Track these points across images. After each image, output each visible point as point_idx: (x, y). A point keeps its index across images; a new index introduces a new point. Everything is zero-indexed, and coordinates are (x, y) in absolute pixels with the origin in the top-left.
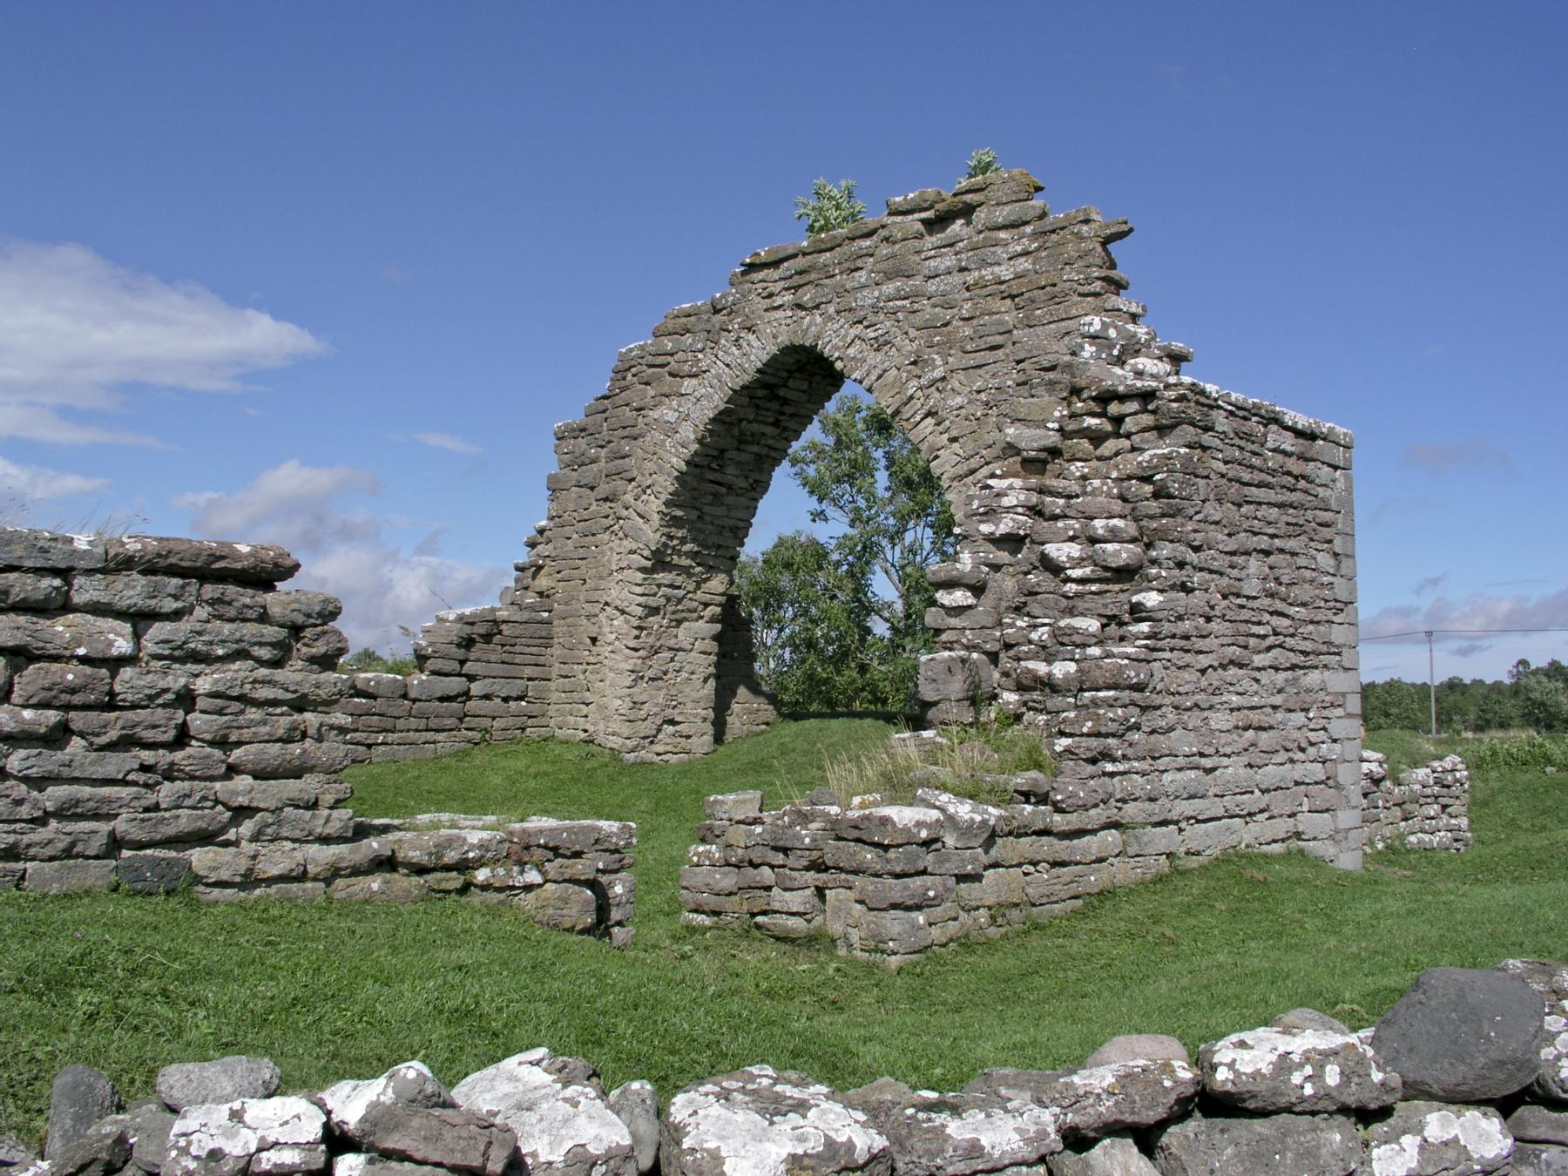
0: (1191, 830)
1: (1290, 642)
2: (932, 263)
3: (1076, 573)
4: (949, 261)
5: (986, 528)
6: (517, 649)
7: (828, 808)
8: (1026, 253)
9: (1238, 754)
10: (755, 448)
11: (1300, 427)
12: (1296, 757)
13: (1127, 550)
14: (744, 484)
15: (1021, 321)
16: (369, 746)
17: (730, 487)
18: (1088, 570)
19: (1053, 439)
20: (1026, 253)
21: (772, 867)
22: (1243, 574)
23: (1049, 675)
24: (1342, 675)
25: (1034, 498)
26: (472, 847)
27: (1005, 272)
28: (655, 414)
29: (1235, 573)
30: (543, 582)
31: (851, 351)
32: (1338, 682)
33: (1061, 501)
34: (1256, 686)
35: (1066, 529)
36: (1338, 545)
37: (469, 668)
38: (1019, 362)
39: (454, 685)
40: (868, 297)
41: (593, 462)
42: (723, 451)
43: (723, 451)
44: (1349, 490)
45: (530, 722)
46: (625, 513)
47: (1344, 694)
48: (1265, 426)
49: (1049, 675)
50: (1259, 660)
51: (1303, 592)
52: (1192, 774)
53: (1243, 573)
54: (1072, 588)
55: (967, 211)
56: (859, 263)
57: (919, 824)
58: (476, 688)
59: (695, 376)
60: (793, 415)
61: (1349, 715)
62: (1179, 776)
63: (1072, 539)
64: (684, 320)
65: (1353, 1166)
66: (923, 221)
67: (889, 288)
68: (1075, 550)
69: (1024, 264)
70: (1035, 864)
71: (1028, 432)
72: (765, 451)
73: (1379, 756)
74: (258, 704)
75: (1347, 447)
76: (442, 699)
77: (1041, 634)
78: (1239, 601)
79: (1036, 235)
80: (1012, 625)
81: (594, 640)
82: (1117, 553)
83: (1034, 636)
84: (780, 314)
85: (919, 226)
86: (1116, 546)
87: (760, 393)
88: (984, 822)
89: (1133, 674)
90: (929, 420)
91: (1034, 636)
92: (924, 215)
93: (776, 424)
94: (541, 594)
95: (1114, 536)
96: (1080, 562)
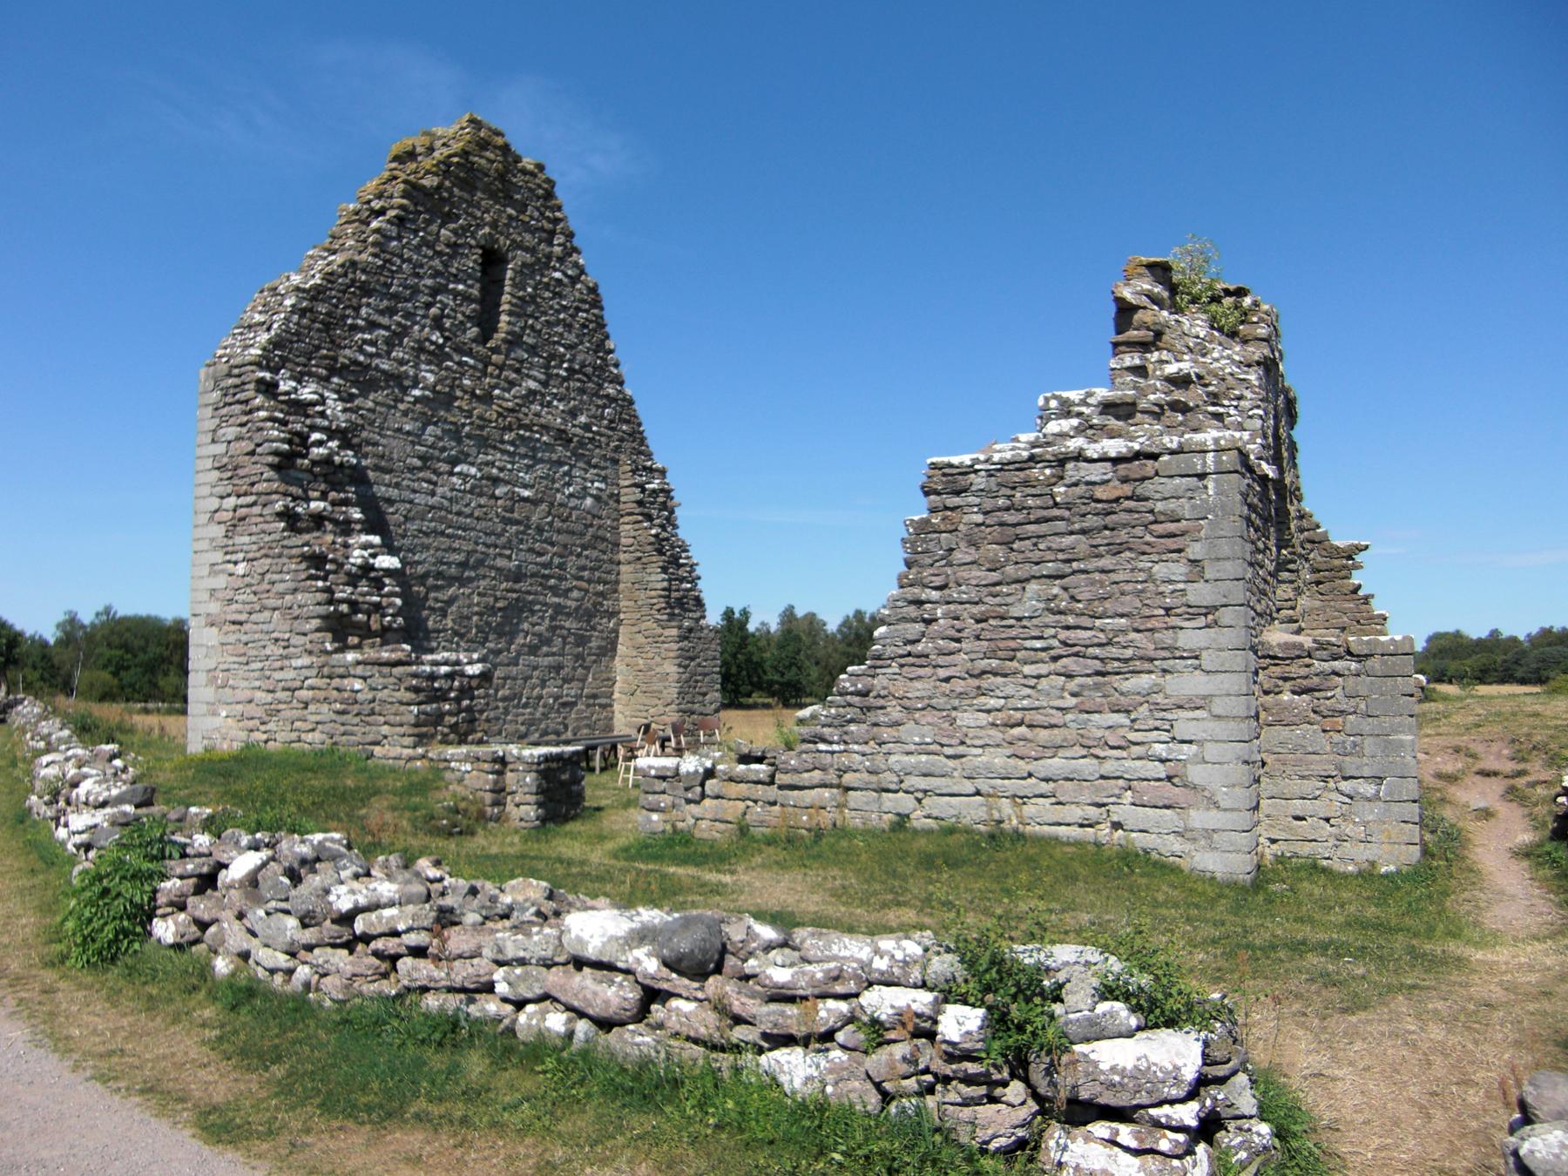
11: (1113, 454)
52: (924, 758)
57: (650, 767)
78: (1005, 623)
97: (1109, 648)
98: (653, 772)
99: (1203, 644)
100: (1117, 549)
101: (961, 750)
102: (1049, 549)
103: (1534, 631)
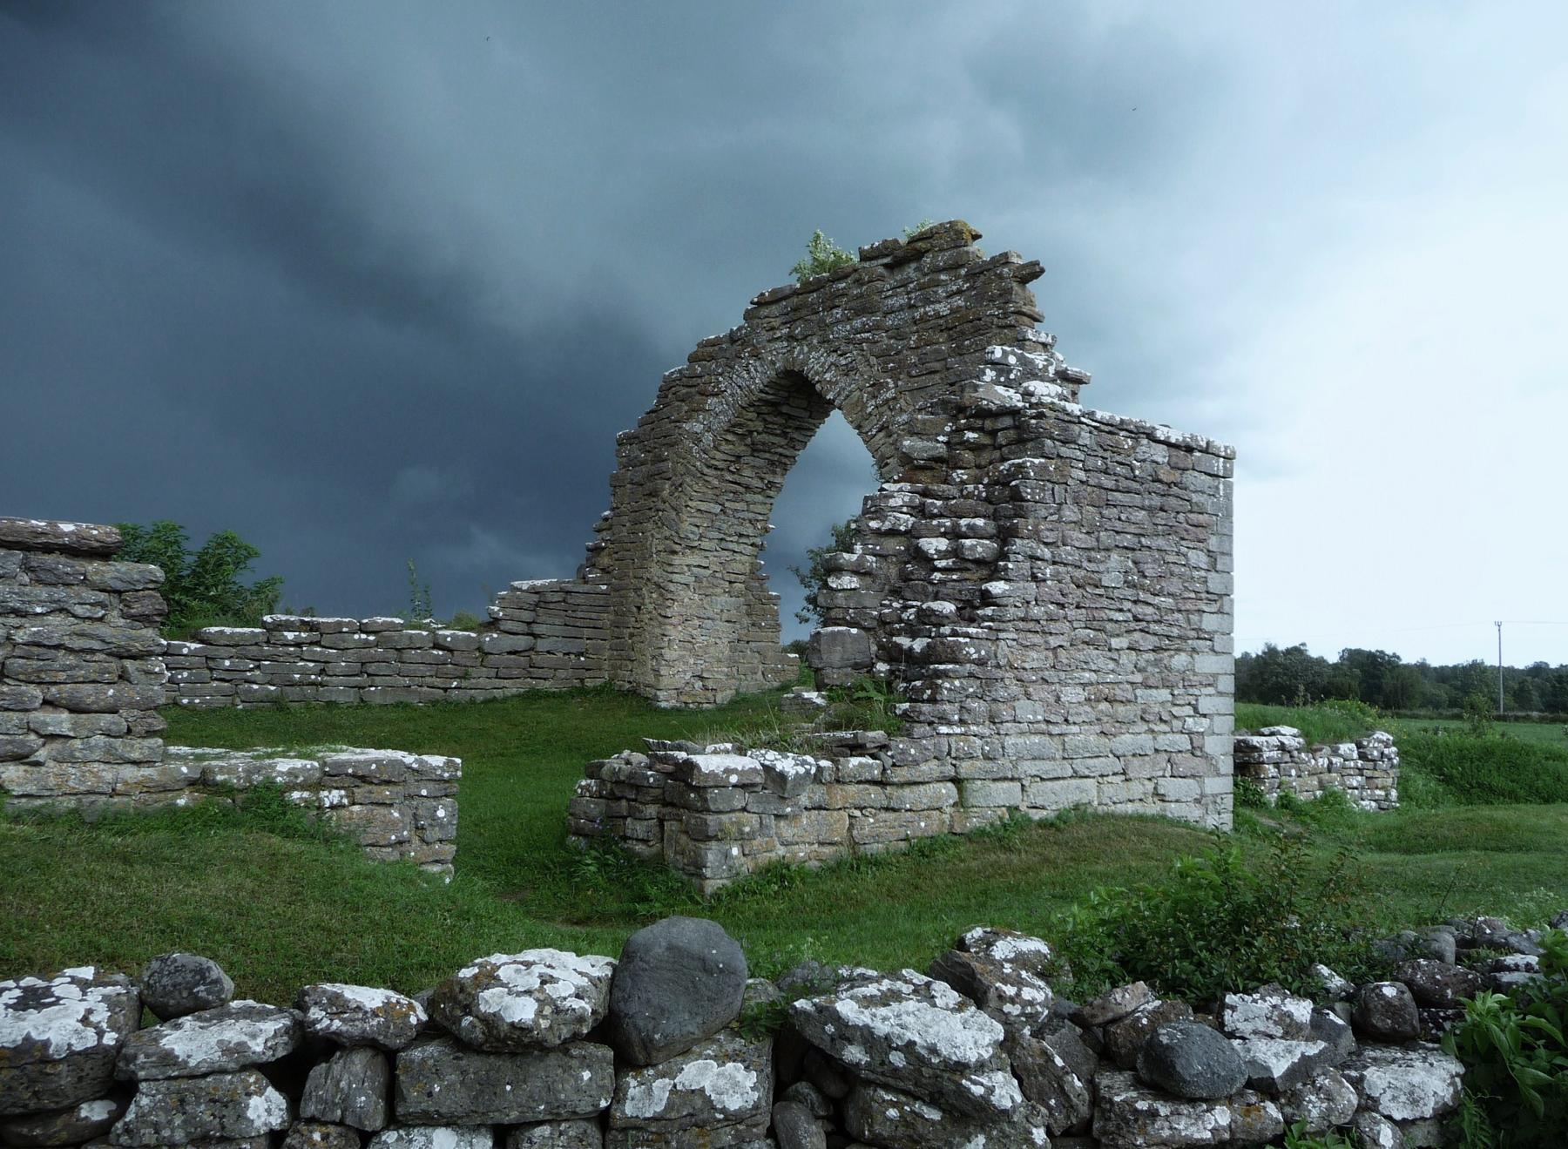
0: (1035, 788)
1: (1154, 627)
2: (890, 302)
3: (941, 564)
4: (903, 300)
5: (874, 524)
6: (580, 615)
7: (676, 753)
8: (959, 292)
9: (1091, 723)
10: (767, 455)
11: (1173, 441)
12: (1156, 728)
13: (982, 545)
14: (760, 485)
15: (953, 350)
16: (445, 690)
17: (747, 488)
18: (950, 562)
19: (942, 450)
20: (959, 292)
21: (629, 800)
22: (1102, 568)
23: (911, 649)
24: (1214, 658)
25: (917, 500)
26: (281, 774)
27: (943, 308)
28: (686, 426)
29: (1092, 566)
30: (605, 561)
31: (827, 376)
32: (1207, 664)
33: (939, 503)
34: (1112, 665)
35: (940, 525)
36: (1213, 543)
37: (537, 629)
38: (952, 385)
39: (522, 642)
40: (843, 330)
41: (642, 464)
42: (739, 457)
43: (739, 457)
44: (1228, 496)
45: (587, 674)
46: (661, 506)
47: (1215, 676)
48: (1136, 440)
49: (911, 649)
50: (1115, 643)
51: (1174, 586)
52: (1036, 739)
53: (1102, 568)
54: (937, 576)
55: (918, 255)
56: (837, 302)
57: (728, 771)
58: (542, 645)
59: (716, 395)
60: (798, 429)
61: (1220, 694)
62: (1021, 740)
63: (943, 535)
64: (710, 349)
65: (603, 1104)
66: (885, 266)
67: (857, 323)
68: (943, 544)
69: (959, 302)
70: (861, 809)
71: (919, 444)
72: (776, 458)
73: (1295, 731)
74: (71, 651)
75: (1228, 458)
76: (509, 653)
77: (910, 614)
78: (1097, 591)
79: (967, 277)
80: (890, 606)
81: (639, 608)
82: (973, 548)
83: (904, 616)
84: (778, 345)
85: (881, 270)
86: (974, 541)
87: (764, 409)
88: (808, 772)
89: (972, 650)
90: (881, 435)
91: (904, 616)
92: (886, 261)
93: (784, 435)
94: (603, 570)
95: (974, 532)
96: (943, 555)
97: (97, 625)
98: (734, 779)
99: (1215, 628)
100: (1170, 530)
101: (1064, 728)
102: (1128, 521)
103: (1389, 652)
